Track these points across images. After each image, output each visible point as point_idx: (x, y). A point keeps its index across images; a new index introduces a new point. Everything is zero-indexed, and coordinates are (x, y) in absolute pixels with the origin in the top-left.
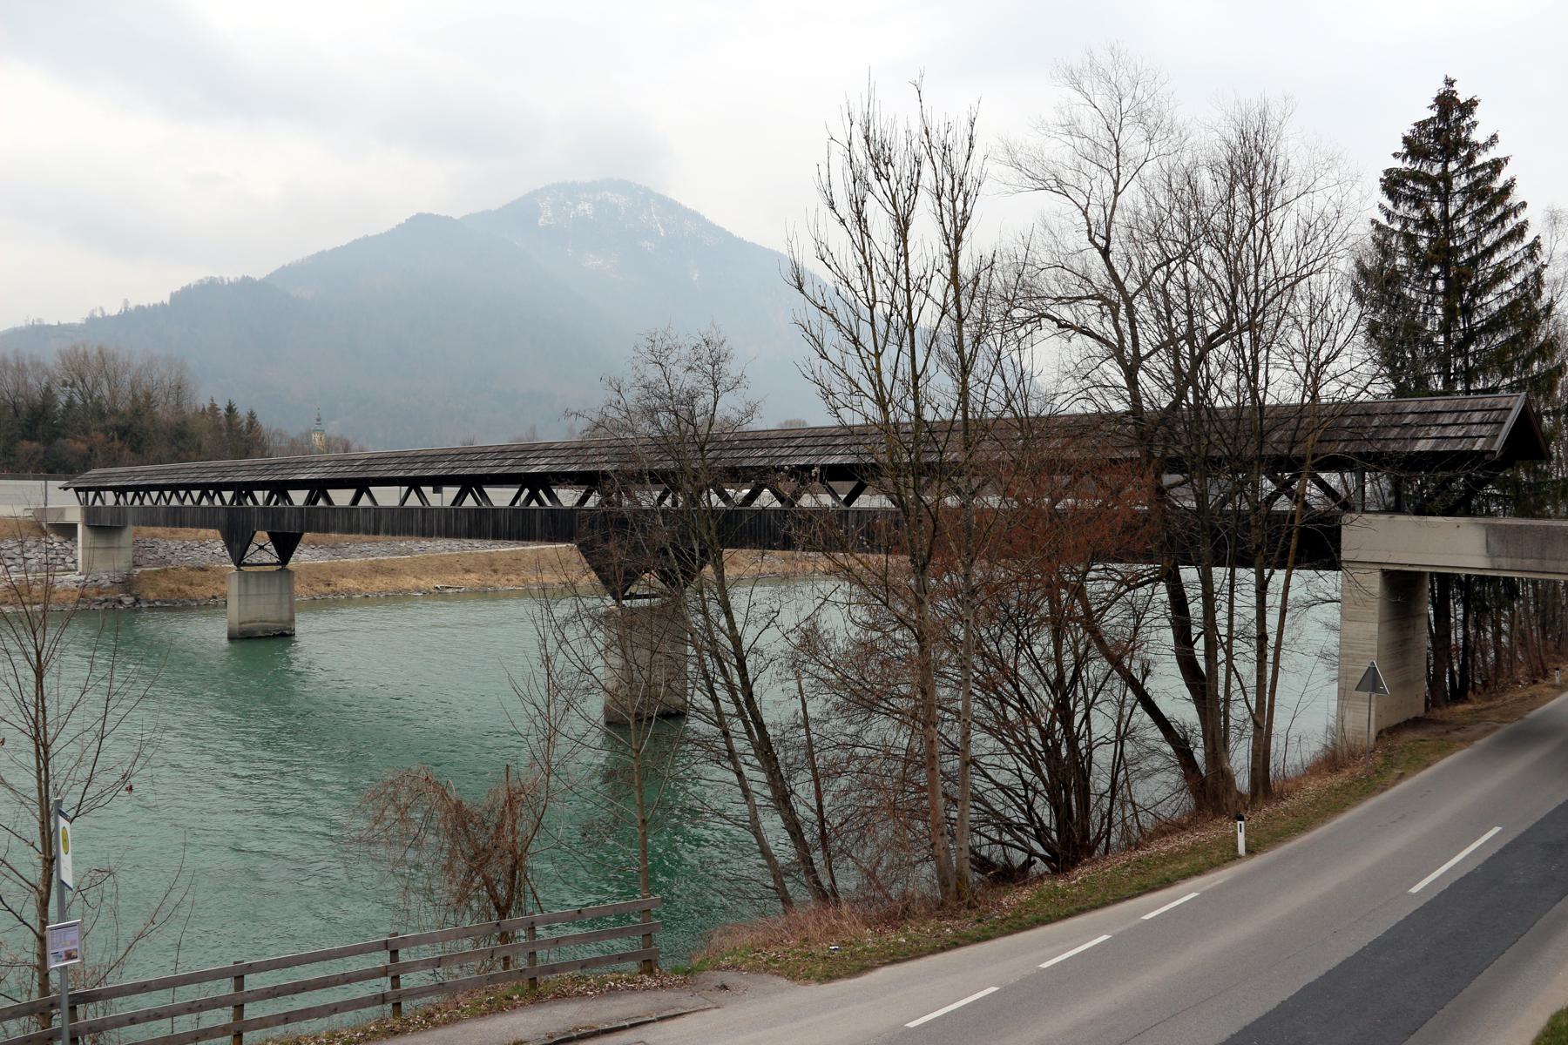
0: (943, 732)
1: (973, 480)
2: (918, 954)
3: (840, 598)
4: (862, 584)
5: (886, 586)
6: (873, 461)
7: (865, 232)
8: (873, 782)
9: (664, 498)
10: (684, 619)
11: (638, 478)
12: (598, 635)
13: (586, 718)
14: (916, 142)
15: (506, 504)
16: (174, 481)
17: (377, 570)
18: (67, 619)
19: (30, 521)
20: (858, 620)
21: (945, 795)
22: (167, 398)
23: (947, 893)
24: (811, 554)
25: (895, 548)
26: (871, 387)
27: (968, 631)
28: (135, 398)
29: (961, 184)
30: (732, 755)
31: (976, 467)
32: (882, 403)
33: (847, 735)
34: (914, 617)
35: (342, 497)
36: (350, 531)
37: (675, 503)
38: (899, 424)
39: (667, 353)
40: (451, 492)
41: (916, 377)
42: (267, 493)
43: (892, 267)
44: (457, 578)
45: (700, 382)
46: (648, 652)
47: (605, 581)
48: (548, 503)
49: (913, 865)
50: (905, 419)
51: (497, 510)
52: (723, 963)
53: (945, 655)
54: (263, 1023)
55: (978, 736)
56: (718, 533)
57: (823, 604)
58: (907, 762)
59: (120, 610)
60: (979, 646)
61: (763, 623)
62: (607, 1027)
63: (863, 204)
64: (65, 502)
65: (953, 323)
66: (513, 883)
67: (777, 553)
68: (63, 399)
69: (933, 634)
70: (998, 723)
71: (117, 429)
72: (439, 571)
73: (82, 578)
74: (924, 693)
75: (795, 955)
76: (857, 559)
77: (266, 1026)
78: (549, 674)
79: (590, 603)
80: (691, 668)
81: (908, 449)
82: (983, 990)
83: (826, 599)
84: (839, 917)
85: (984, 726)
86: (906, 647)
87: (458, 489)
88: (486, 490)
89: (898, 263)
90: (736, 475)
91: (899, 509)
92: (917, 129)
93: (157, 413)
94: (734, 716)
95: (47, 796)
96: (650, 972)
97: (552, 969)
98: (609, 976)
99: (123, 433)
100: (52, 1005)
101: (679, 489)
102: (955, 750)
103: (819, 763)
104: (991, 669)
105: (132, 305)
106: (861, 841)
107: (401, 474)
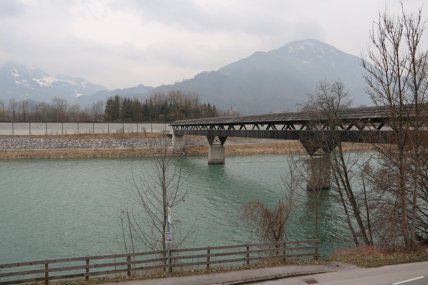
0: (407, 197)
1: (419, 122)
2: (397, 263)
3: (376, 156)
4: (383, 153)
5: (390, 153)
6: (387, 117)
7: (384, 49)
8: (385, 211)
9: (325, 127)
10: (330, 161)
11: (317, 122)
12: (306, 165)
13: (302, 188)
14: (401, 20)
15: (281, 129)
16: (195, 124)
17: (246, 147)
18: (171, 157)
19: (162, 134)
20: (381, 163)
21: (407, 216)
22: (194, 102)
23: (407, 246)
24: (367, 144)
25: (393, 142)
26: (386, 95)
27: (416, 168)
28: (186, 103)
29: (416, 32)
30: (343, 200)
31: (420, 118)
32: (390, 99)
33: (377, 197)
34: (399, 163)
35: (237, 128)
36: (239, 136)
37: (328, 129)
38: (395, 106)
39: (325, 87)
40: (266, 126)
41: (400, 92)
42: (218, 126)
43: (393, 59)
44: (267, 149)
45: (335, 95)
46: (319, 171)
47: (308, 151)
48: (292, 129)
49: (396, 236)
50: (397, 104)
51: (278, 131)
52: (338, 259)
53: (409, 174)
54: (214, 262)
55: (419, 199)
56: (340, 137)
57: (371, 158)
58: (395, 205)
59: (182, 156)
60: (420, 172)
61: (353, 163)
62: (304, 273)
63: (384, 41)
64: (169, 129)
65: (413, 75)
66: (280, 232)
67: (357, 143)
68: (169, 103)
69: (404, 168)
70: (426, 196)
71: (182, 110)
72: (262, 147)
73: (174, 148)
74: (401, 185)
75: (359, 259)
76: (381, 145)
77: (215, 263)
78: (292, 176)
79: (304, 156)
80: (331, 175)
81: (398, 113)
82: (419, 277)
83: (372, 157)
84: (373, 249)
85: (421, 196)
86: (396, 172)
87: (268, 125)
88: (275, 125)
89: (395, 58)
90: (345, 121)
91: (394, 131)
92: (401, 16)
93: (191, 106)
94: (344, 189)
95: (165, 201)
96: (317, 260)
97: (290, 256)
98: (305, 260)
99: (183, 111)
100: (166, 252)
101: (329, 125)
102: (411, 203)
103: (368, 204)
104: (424, 179)
105: (185, 79)
106: (380, 228)
107: (253, 121)
